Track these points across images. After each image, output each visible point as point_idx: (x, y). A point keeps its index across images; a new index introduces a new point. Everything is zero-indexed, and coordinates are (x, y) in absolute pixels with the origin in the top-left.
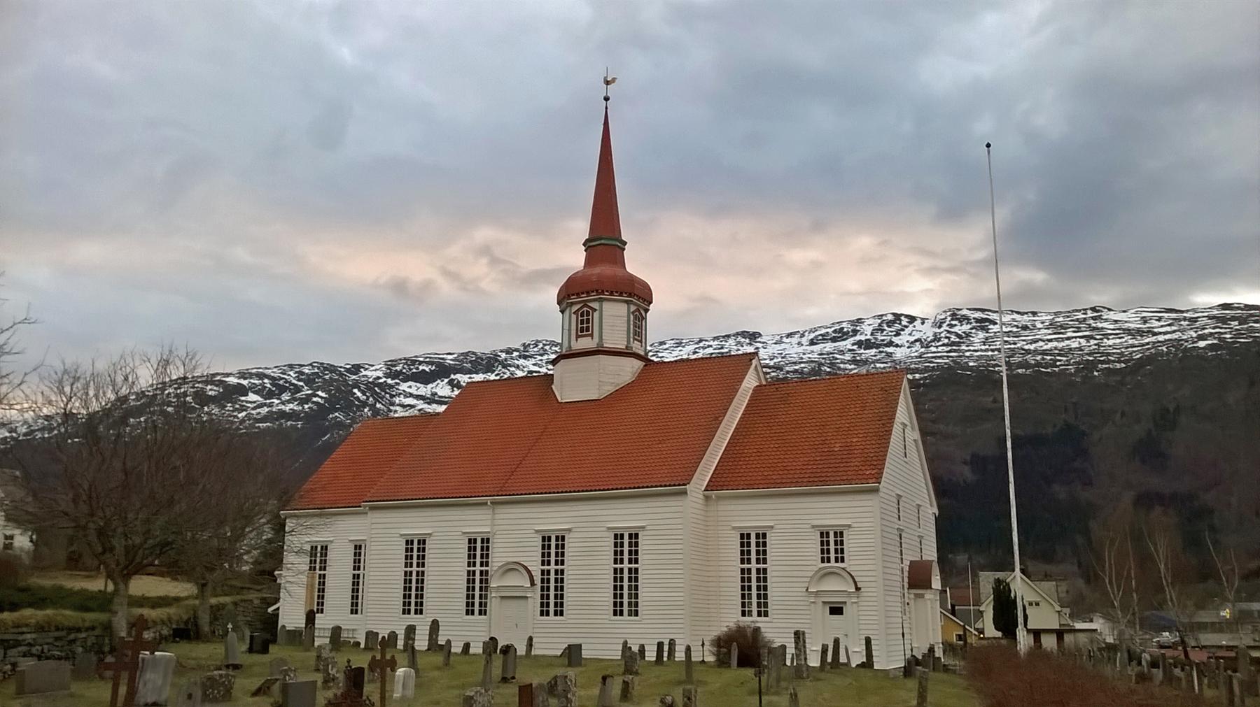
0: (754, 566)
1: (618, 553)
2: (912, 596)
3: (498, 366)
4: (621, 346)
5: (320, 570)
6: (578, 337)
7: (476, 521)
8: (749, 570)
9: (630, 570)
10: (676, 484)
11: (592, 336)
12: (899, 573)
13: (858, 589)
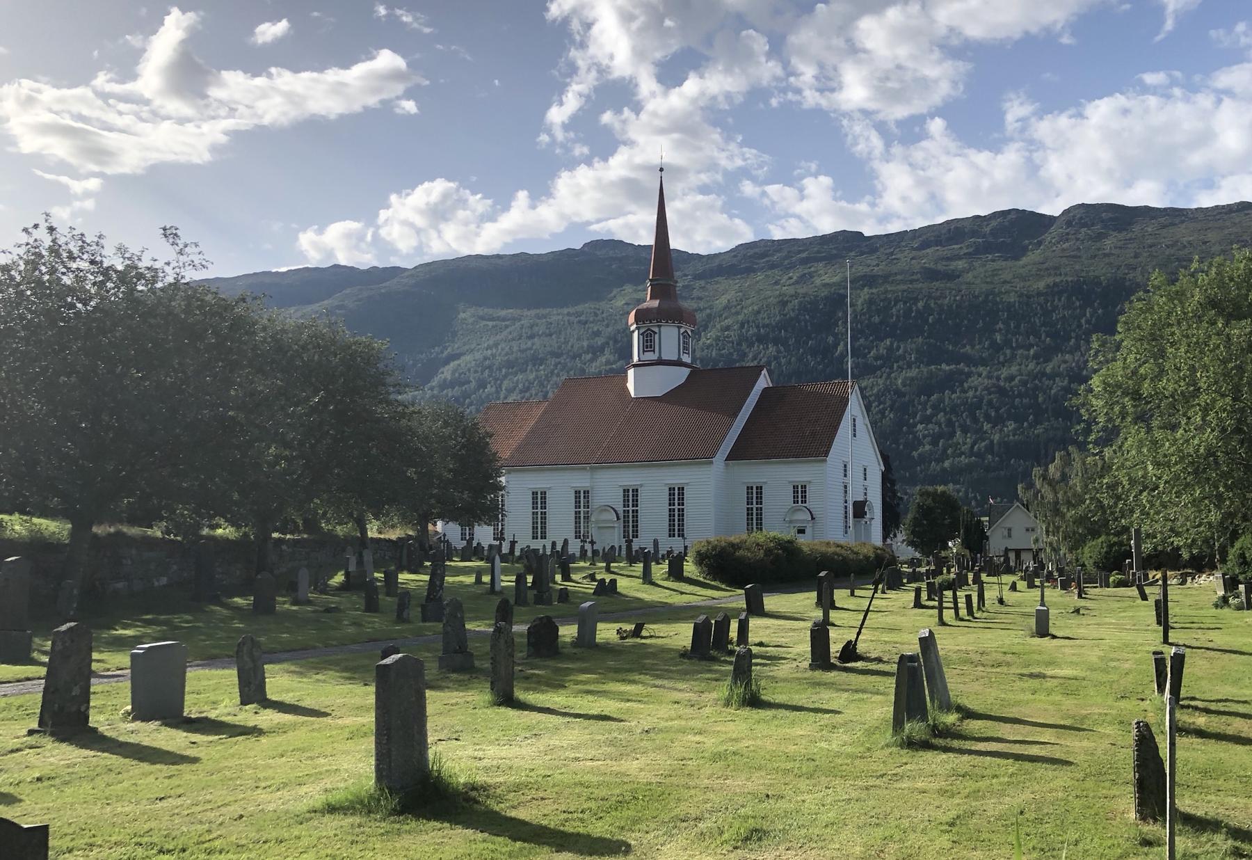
0: (755, 506)
1: (535, 503)
3: (264, 341)
4: (675, 358)
5: (633, 506)
6: (644, 351)
7: (580, 480)
9: (679, 509)
10: (706, 456)
11: (654, 351)
13: (813, 518)
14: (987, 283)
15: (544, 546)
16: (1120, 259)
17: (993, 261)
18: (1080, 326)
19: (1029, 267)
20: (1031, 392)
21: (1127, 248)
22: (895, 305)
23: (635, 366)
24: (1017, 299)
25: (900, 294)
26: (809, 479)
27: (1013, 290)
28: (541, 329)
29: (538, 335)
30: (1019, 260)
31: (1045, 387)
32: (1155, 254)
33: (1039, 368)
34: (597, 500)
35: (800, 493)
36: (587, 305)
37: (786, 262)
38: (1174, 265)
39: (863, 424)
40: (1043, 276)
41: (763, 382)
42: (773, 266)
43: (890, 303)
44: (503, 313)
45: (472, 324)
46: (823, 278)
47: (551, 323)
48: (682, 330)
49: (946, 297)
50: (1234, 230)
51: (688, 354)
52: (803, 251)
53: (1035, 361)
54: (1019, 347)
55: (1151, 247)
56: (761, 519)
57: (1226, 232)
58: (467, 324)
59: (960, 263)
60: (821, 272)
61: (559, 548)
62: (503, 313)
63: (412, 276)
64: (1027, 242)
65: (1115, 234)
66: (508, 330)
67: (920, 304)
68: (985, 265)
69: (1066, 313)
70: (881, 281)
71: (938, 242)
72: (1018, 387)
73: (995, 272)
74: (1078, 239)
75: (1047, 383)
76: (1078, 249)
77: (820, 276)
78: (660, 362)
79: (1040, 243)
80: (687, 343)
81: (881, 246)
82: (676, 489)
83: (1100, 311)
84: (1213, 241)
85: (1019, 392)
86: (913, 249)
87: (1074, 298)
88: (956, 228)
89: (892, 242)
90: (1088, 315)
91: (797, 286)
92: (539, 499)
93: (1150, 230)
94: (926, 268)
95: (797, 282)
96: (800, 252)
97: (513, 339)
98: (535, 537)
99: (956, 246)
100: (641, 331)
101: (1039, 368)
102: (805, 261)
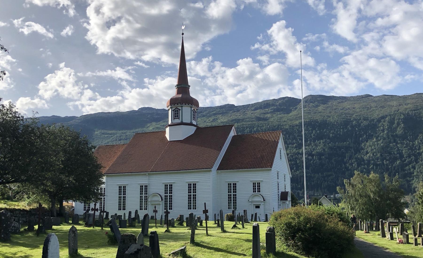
0: (232, 193)
2: (282, 203)
6: (174, 119)
7: (143, 180)
8: (191, 195)
10: (208, 168)
11: (179, 118)
12: (277, 195)
13: (264, 200)
14: (278, 122)
15: (125, 214)
16: (324, 113)
17: (280, 114)
18: (311, 137)
19: (293, 116)
20: (294, 159)
21: (327, 110)
22: (246, 129)
23: (170, 126)
24: (289, 127)
25: (248, 125)
26: (262, 180)
27: (287, 124)
28: (124, 137)
29: (122, 139)
30: (289, 114)
31: (299, 157)
32: (337, 112)
33: (297, 151)
34: (151, 190)
35: (257, 187)
36: (139, 129)
37: (208, 115)
38: (343, 116)
39: (284, 152)
40: (298, 119)
41: (233, 133)
42: (204, 116)
43: (244, 128)
44: (110, 132)
45: (100, 136)
46: (221, 120)
47: (127, 135)
48: (193, 109)
49: (264, 126)
50: (364, 104)
51: (195, 120)
52: (214, 111)
53: (295, 149)
54: (290, 144)
55: (335, 109)
56: (236, 200)
57: (361, 104)
58: (98, 136)
59: (268, 115)
60: (220, 118)
61: (133, 216)
62: (110, 132)
63: (80, 119)
64: (292, 108)
65: (322, 105)
66: (112, 138)
67: (255, 129)
68: (277, 116)
69: (306, 132)
70: (241, 121)
71: (260, 108)
72: (290, 157)
73: (281, 118)
74: (309, 107)
75: (300, 156)
76: (310, 110)
77: (220, 119)
78: (182, 124)
79: (296, 108)
80: (195, 115)
81: (241, 109)
82: (192, 185)
83: (318, 132)
84: (357, 108)
85: (290, 159)
86: (253, 110)
87: (309, 127)
88: (267, 103)
89: (244, 108)
90: (314, 133)
91: (212, 123)
92: (122, 190)
93: (334, 104)
94: (257, 117)
95: (212, 122)
96: (213, 111)
97: (114, 141)
98: (120, 209)
99: (266, 109)
100: (173, 109)
101: (297, 151)
102: (214, 114)
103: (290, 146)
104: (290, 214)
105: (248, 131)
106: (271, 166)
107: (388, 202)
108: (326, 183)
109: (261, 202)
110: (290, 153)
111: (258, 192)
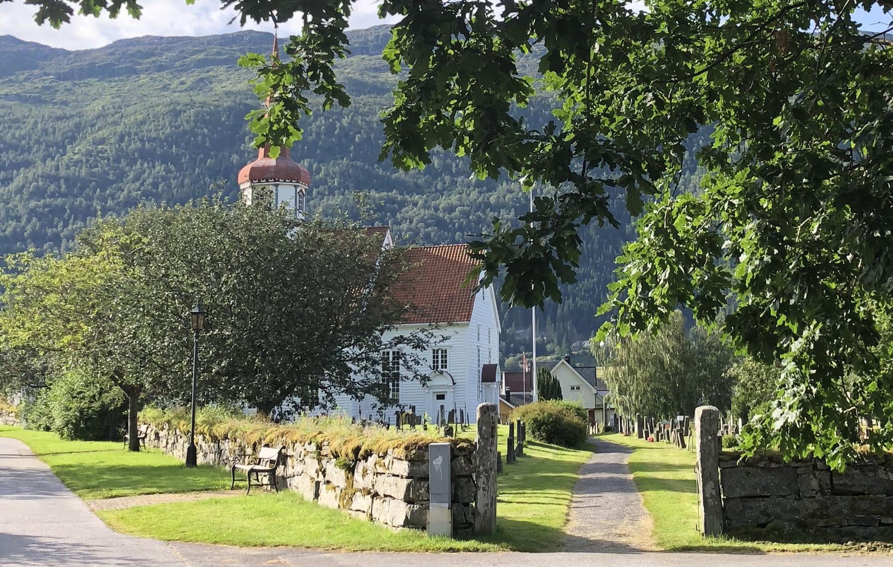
2: (484, 386)
12: (477, 373)
22: (314, 121)
42: (161, 68)
46: (224, 84)
52: (202, 51)
75: (491, 214)
77: (220, 81)
91: (191, 93)
94: (351, 78)
95: (191, 89)
96: (195, 52)
102: (201, 64)
103: (460, 179)
104: (535, 410)
105: (323, 128)
106: (468, 318)
107: (703, 373)
108: (571, 299)
109: (449, 387)
110: (458, 203)
111: (442, 367)
